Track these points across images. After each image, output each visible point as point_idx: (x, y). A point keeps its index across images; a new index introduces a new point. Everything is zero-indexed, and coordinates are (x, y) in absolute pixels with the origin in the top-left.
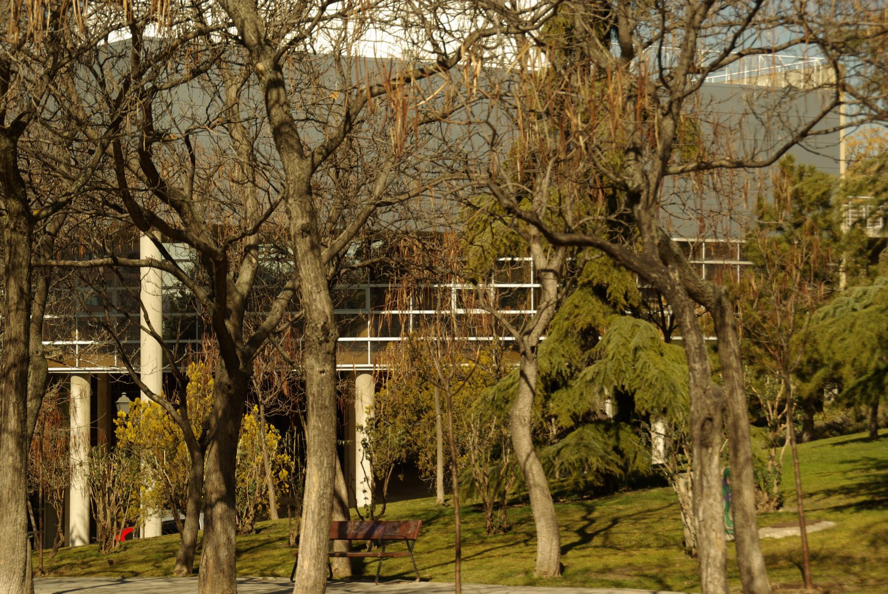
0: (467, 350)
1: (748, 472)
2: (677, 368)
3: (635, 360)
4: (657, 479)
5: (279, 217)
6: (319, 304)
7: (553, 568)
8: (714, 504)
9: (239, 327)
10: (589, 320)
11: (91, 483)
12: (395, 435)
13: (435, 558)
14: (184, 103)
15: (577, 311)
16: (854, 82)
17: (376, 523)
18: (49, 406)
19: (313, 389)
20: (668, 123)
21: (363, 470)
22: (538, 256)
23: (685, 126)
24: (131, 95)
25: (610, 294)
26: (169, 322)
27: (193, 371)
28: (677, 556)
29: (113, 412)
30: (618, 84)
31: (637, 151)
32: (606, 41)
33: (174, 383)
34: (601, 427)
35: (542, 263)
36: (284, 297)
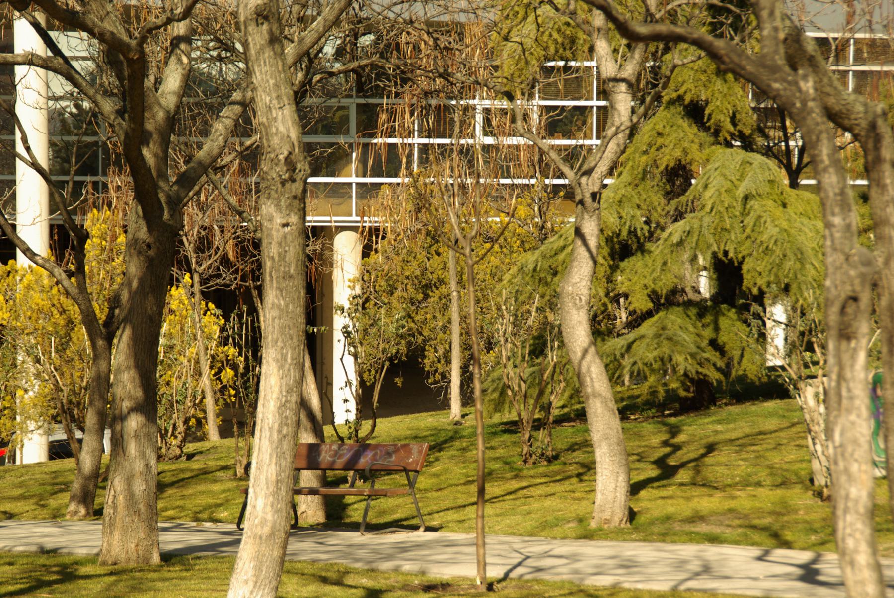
3: (745, 213)
4: (774, 388)
6: (281, 126)
7: (618, 515)
9: (164, 159)
12: (391, 321)
13: (447, 498)
15: (660, 141)
17: (363, 446)
19: (271, 251)
21: (344, 370)
22: (605, 58)
25: (710, 115)
26: (58, 150)
27: (95, 223)
28: (801, 499)
33: (66, 239)
34: (693, 311)
35: (609, 69)
36: (229, 114)
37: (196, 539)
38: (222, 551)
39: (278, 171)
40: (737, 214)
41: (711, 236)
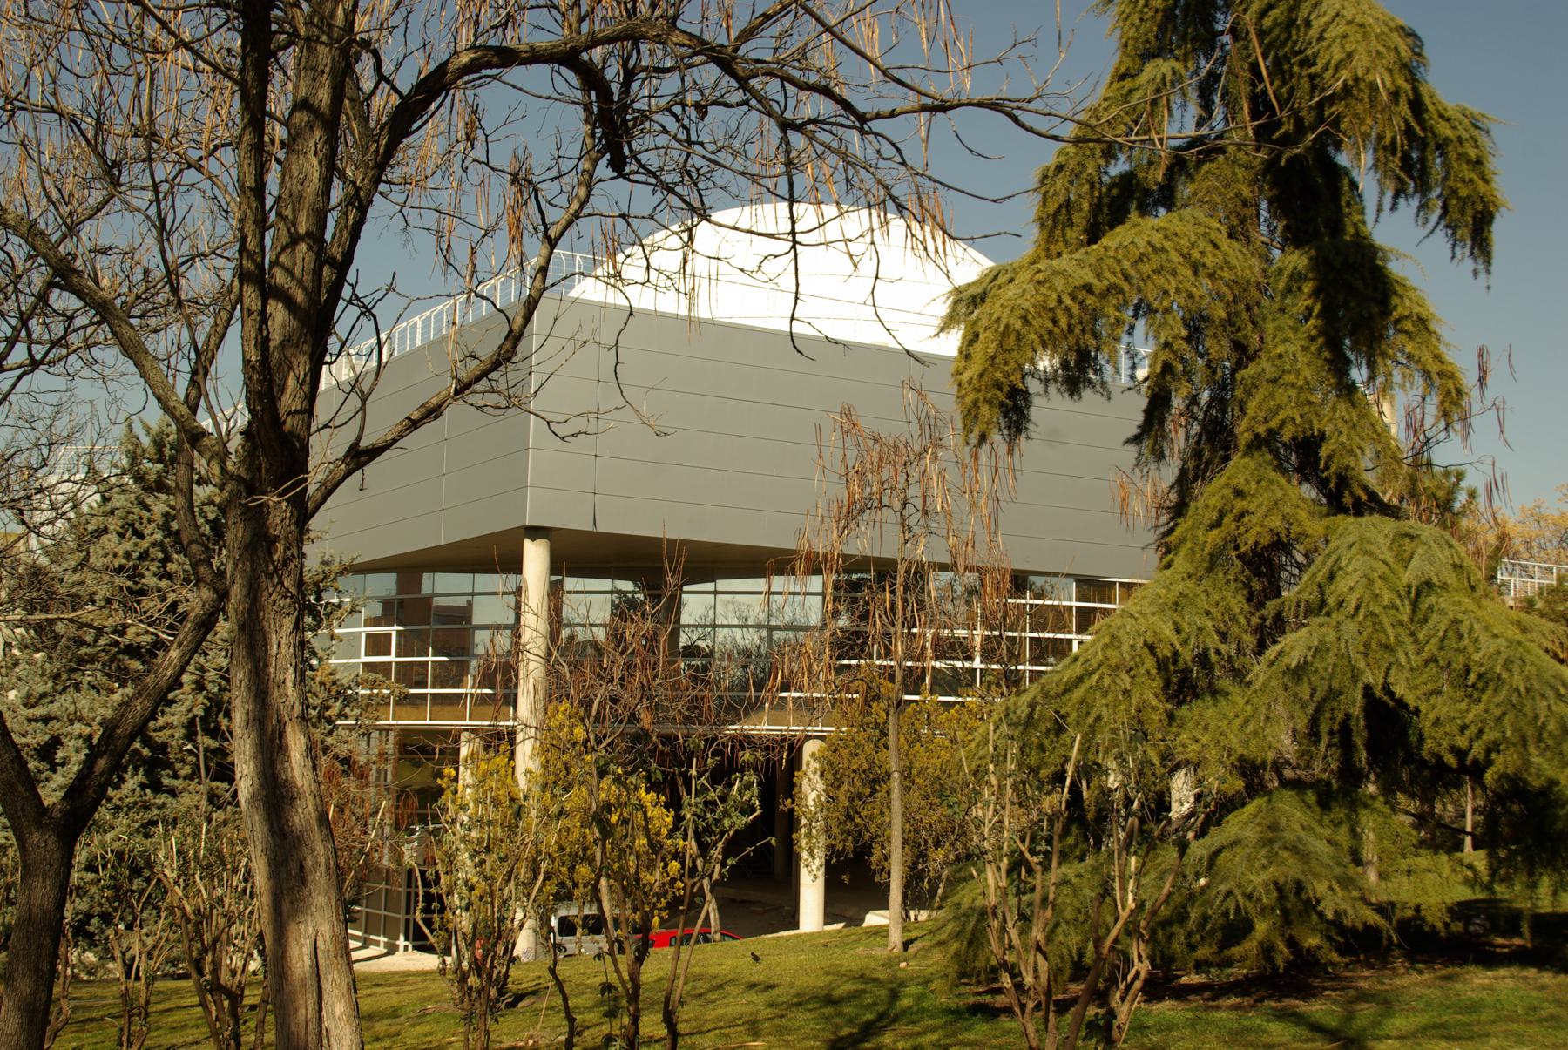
3: (1420, 617)
10: (1275, 522)
15: (1240, 505)
25: (1330, 457)
34: (1311, 797)
40: (1405, 618)
41: (1360, 656)
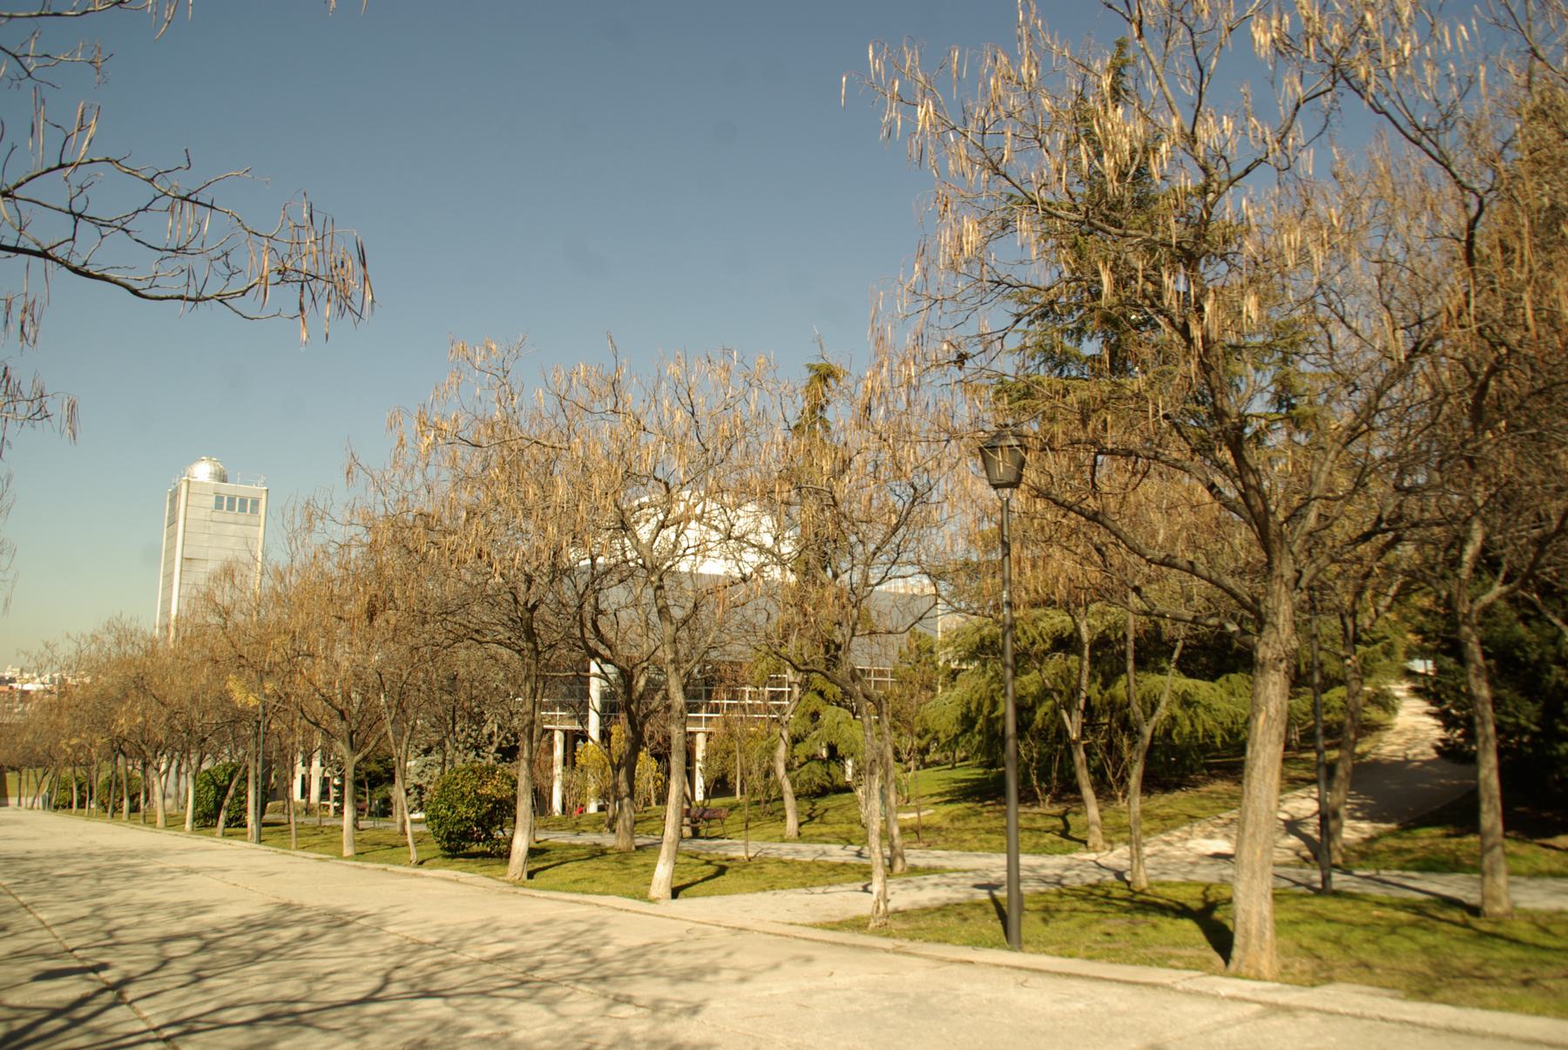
0: (753, 722)
1: (893, 786)
2: (860, 734)
4: (848, 789)
5: (659, 653)
6: (678, 699)
7: (795, 834)
8: (876, 803)
9: (638, 709)
11: (563, 784)
12: (716, 765)
13: (735, 828)
14: (615, 596)
16: (944, 593)
17: (705, 810)
18: (544, 745)
19: (674, 742)
20: (855, 612)
21: (699, 782)
22: (789, 675)
23: (863, 612)
24: (589, 592)
26: (604, 705)
27: (615, 730)
28: (857, 828)
29: (575, 749)
30: (830, 592)
31: (840, 624)
32: (824, 569)
33: (605, 735)
35: (792, 679)
36: (661, 693)
37: (647, 841)
38: (656, 846)
39: (677, 715)
